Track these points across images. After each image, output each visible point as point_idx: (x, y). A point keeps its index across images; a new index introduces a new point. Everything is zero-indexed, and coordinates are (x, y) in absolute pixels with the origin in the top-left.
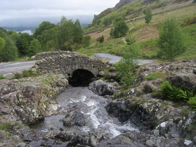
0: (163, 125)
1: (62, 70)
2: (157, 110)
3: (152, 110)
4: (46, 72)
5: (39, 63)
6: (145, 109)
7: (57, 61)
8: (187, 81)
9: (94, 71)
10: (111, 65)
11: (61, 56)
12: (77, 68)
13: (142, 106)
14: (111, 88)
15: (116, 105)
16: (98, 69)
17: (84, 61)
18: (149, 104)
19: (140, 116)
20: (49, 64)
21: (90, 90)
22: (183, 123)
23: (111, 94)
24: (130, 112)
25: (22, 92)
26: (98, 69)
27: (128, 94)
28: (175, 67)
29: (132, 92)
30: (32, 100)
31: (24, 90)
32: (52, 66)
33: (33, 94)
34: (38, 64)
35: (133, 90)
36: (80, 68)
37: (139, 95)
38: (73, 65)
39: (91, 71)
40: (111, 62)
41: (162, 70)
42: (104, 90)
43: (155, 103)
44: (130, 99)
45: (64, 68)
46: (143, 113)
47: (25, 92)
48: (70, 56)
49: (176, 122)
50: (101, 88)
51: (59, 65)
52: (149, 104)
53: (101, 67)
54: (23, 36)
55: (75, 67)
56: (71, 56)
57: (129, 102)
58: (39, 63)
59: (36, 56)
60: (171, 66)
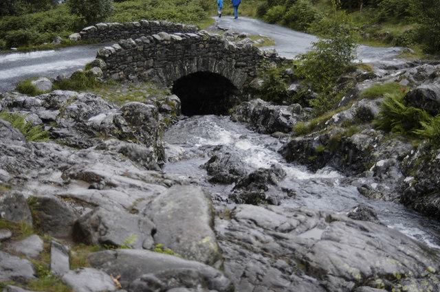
0: (381, 163)
1: (158, 74)
2: (375, 146)
3: (366, 146)
4: (121, 76)
5: (107, 55)
6: (355, 145)
7: (148, 49)
8: (431, 97)
9: (238, 78)
10: (281, 61)
11: (157, 36)
12: (195, 69)
13: (349, 140)
14: (287, 117)
15: (300, 145)
16: (248, 72)
17: (213, 52)
18: (363, 136)
19: (346, 157)
20: (130, 59)
21: (235, 121)
22: (409, 159)
23: (286, 130)
24: (328, 153)
25: (122, 115)
26: (248, 72)
27: (326, 123)
28: (430, 73)
29: (333, 120)
30: (145, 129)
31: (126, 112)
32: (135, 63)
33: (146, 119)
34: (104, 58)
35: (336, 117)
36: (203, 69)
37: (346, 124)
38: (186, 62)
39: (229, 78)
40: (281, 54)
41: (401, 79)
42: (271, 122)
43: (374, 136)
44: (330, 132)
45: (164, 67)
46: (351, 151)
47: (128, 114)
48: (180, 39)
49: (400, 159)
50: (262, 118)
51: (152, 60)
52: (363, 136)
53: (256, 66)
54: (385, 112)
55: (191, 67)
56: (182, 36)
57: (327, 137)
58: (107, 55)
59: (82, 35)
60: (423, 70)
